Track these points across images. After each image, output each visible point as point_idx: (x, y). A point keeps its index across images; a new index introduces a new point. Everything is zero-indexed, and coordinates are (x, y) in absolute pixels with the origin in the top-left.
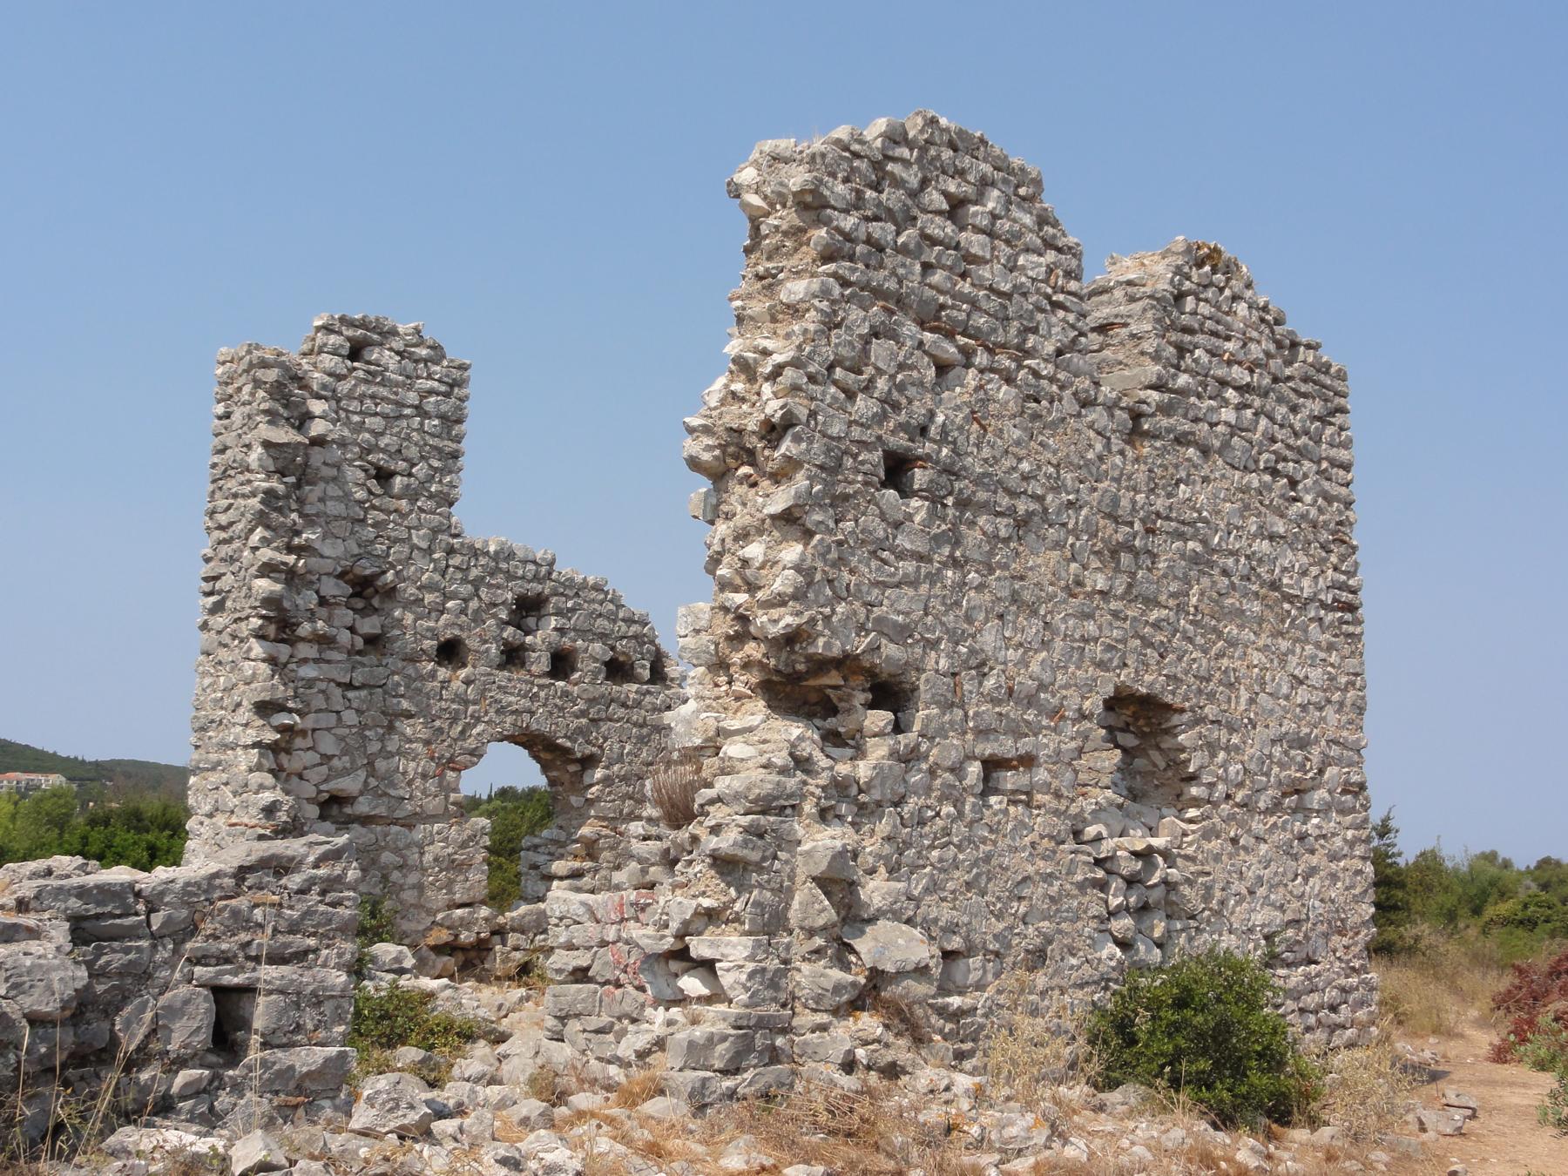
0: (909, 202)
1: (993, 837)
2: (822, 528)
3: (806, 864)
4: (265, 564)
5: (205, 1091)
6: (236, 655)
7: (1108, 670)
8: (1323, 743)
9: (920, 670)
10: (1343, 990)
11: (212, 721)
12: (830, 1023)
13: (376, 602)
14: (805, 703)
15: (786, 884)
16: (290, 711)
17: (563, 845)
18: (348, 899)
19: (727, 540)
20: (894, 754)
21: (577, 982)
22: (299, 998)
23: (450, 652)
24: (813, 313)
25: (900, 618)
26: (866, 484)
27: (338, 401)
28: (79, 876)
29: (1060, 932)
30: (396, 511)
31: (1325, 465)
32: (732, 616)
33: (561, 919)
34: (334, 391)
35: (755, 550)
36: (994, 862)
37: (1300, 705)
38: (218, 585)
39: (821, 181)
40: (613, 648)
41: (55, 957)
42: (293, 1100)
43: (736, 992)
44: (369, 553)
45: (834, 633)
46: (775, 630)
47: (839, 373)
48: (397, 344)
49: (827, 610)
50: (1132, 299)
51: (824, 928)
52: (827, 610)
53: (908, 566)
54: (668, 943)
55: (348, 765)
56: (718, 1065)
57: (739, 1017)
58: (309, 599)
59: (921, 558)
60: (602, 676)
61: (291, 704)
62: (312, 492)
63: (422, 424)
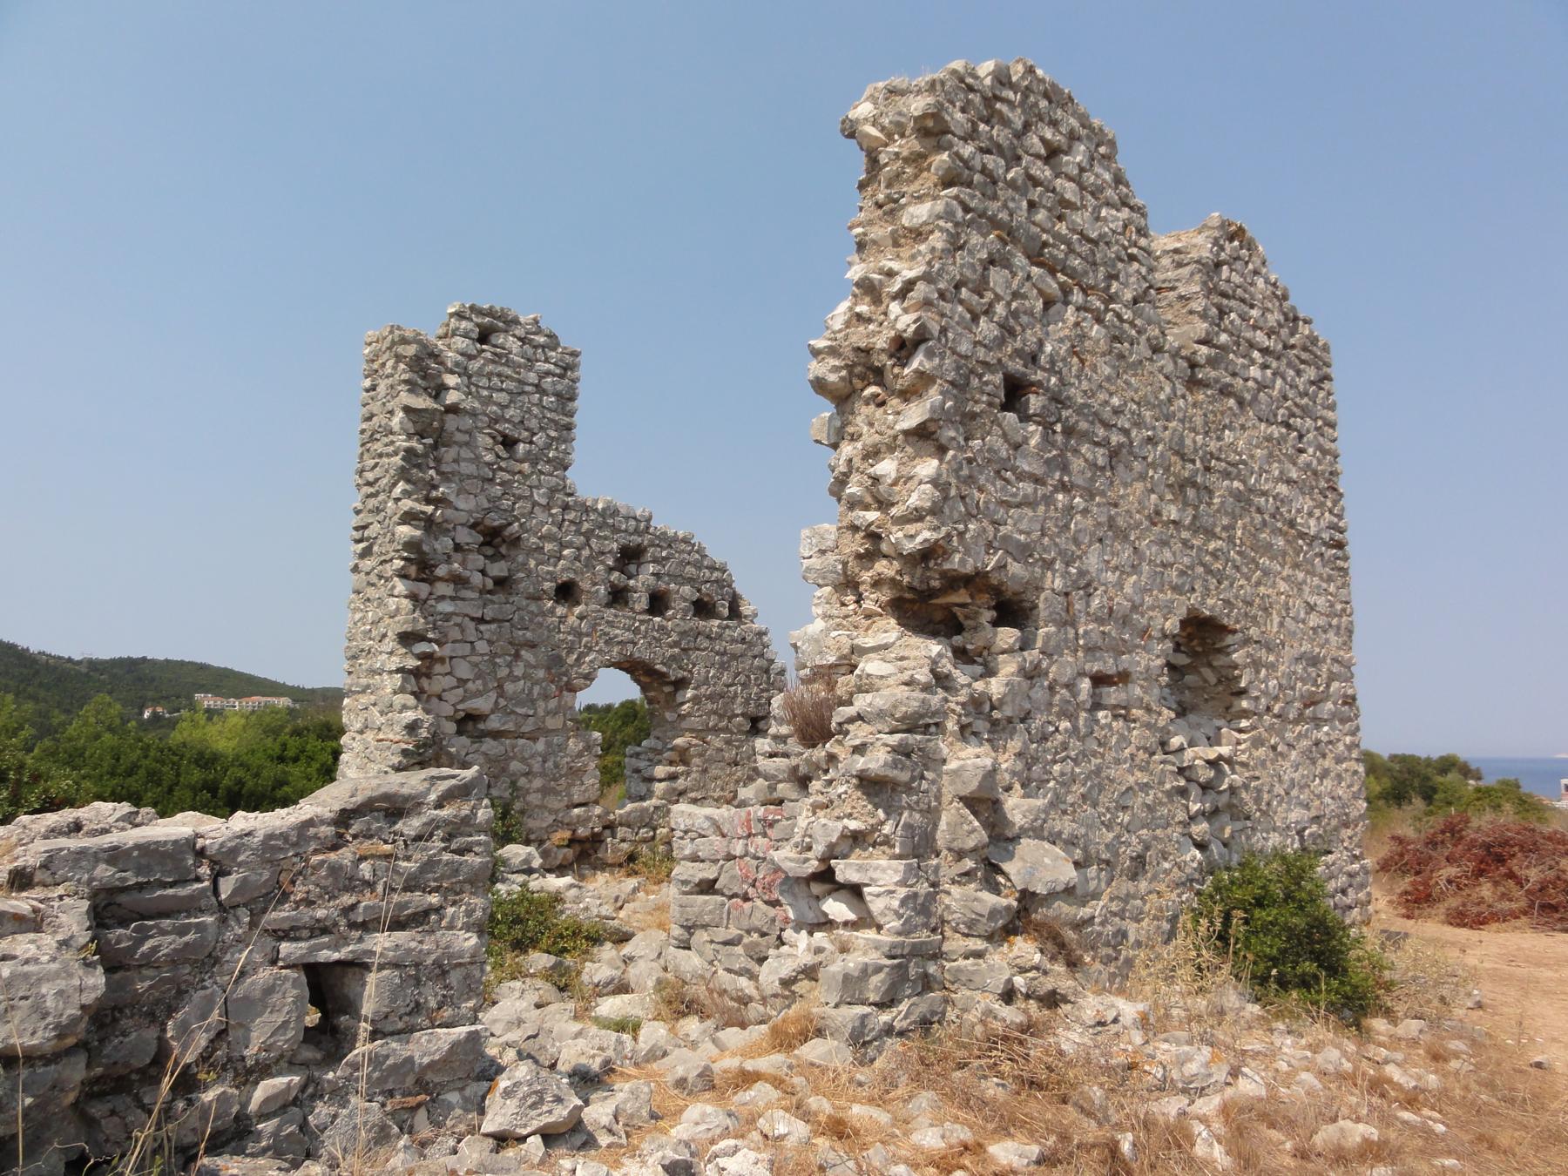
0: (1015, 142)
1: (1101, 750)
2: (954, 444)
3: (952, 783)
4: (406, 513)
5: (295, 1102)
6: (382, 592)
7: (1181, 595)
8: (1329, 661)
9: (1039, 589)
10: (1351, 875)
11: (362, 651)
12: (986, 949)
13: (503, 550)
14: (930, 622)
15: (934, 804)
16: (430, 641)
17: (660, 753)
18: (479, 843)
19: (855, 460)
20: (1022, 671)
21: (702, 892)
22: (418, 970)
23: (566, 592)
24: (937, 234)
25: (1022, 537)
26: (990, 404)
27: (470, 377)
28: (123, 829)
29: (1155, 838)
30: (520, 472)
31: (1320, 423)
32: (862, 534)
33: (686, 832)
34: (466, 368)
35: (887, 467)
36: (1103, 775)
37: (1312, 628)
38: (366, 533)
39: (942, 105)
40: (699, 590)
41: (53, 959)
42: (412, 1101)
43: (887, 919)
44: (497, 507)
45: (967, 552)
46: (910, 547)
47: (964, 292)
48: (520, 332)
49: (961, 527)
50: (1180, 265)
51: (974, 850)
52: (961, 527)
53: (1027, 487)
54: (813, 866)
55: (481, 688)
56: (873, 997)
57: (894, 946)
58: (444, 544)
59: (1038, 480)
60: (691, 613)
61: (430, 635)
62: (449, 454)
63: (541, 400)
